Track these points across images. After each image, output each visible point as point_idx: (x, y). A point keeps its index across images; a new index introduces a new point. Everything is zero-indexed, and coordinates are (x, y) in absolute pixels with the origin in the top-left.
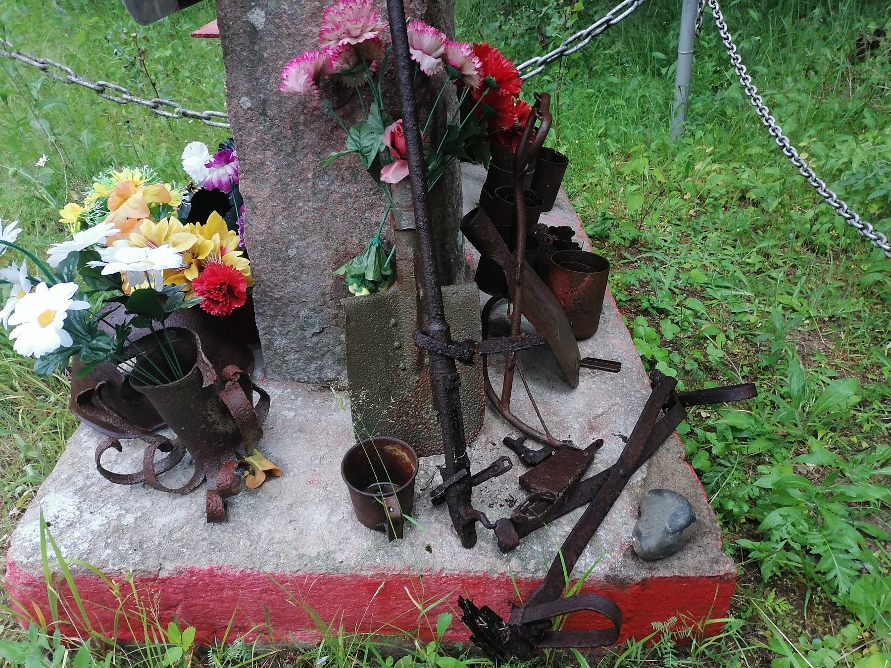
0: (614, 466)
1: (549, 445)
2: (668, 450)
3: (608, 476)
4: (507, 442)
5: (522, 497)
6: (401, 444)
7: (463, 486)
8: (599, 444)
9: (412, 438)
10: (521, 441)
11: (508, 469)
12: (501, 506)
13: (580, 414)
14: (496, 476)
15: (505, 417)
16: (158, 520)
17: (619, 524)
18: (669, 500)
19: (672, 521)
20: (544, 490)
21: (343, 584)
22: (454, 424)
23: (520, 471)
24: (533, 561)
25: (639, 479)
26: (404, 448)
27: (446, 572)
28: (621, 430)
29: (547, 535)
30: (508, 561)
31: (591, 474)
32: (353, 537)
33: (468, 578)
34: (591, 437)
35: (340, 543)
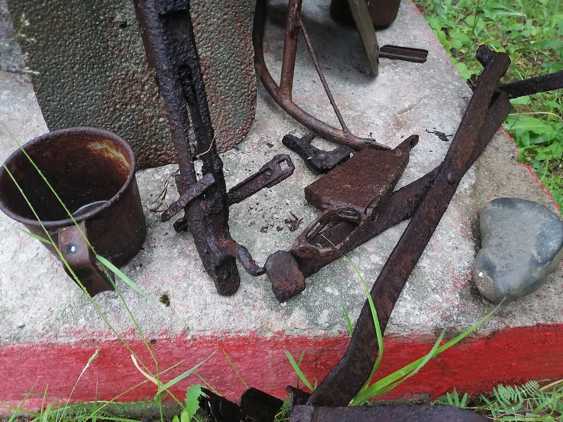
0: (439, 169)
1: (346, 145)
2: (497, 149)
3: (431, 182)
4: (288, 141)
5: (309, 217)
6: (111, 139)
7: (210, 203)
8: (413, 141)
9: (150, 137)
10: (308, 140)
11: (288, 174)
13: (382, 108)
14: (269, 185)
15: (285, 108)
17: (448, 248)
18: (529, 214)
19: (540, 245)
20: (343, 205)
21: (34, 354)
22: (184, 93)
23: (305, 179)
24: (326, 312)
25: (466, 186)
26: (118, 146)
27: (192, 333)
28: (436, 125)
29: (346, 271)
30: (289, 313)
31: (404, 182)
32: (47, 286)
33: (227, 340)
34: (399, 135)
35: (23, 296)
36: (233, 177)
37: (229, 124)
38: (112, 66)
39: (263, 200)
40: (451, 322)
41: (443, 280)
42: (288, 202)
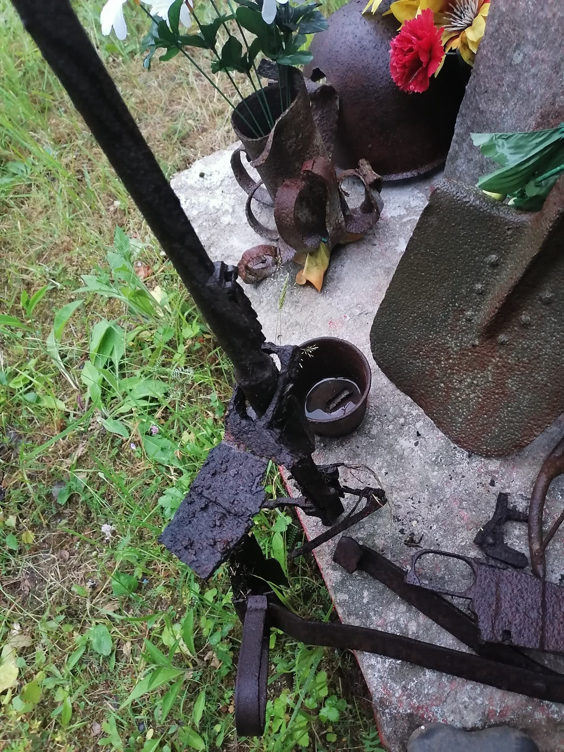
12: (402, 531)
16: (235, 239)
24: (346, 597)
29: (389, 603)
36: (436, 468)
37: (483, 437)
38: (439, 332)
39: (426, 505)
40: (382, 707)
41: (419, 696)
42: (435, 527)
